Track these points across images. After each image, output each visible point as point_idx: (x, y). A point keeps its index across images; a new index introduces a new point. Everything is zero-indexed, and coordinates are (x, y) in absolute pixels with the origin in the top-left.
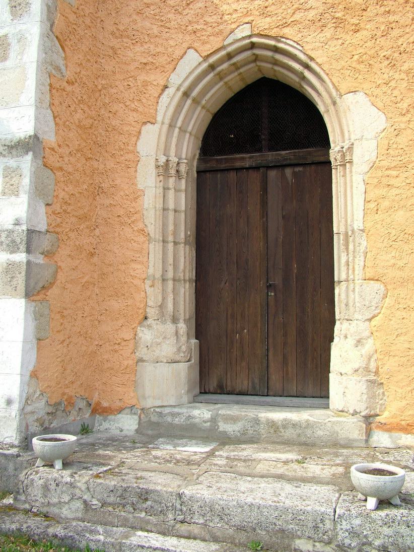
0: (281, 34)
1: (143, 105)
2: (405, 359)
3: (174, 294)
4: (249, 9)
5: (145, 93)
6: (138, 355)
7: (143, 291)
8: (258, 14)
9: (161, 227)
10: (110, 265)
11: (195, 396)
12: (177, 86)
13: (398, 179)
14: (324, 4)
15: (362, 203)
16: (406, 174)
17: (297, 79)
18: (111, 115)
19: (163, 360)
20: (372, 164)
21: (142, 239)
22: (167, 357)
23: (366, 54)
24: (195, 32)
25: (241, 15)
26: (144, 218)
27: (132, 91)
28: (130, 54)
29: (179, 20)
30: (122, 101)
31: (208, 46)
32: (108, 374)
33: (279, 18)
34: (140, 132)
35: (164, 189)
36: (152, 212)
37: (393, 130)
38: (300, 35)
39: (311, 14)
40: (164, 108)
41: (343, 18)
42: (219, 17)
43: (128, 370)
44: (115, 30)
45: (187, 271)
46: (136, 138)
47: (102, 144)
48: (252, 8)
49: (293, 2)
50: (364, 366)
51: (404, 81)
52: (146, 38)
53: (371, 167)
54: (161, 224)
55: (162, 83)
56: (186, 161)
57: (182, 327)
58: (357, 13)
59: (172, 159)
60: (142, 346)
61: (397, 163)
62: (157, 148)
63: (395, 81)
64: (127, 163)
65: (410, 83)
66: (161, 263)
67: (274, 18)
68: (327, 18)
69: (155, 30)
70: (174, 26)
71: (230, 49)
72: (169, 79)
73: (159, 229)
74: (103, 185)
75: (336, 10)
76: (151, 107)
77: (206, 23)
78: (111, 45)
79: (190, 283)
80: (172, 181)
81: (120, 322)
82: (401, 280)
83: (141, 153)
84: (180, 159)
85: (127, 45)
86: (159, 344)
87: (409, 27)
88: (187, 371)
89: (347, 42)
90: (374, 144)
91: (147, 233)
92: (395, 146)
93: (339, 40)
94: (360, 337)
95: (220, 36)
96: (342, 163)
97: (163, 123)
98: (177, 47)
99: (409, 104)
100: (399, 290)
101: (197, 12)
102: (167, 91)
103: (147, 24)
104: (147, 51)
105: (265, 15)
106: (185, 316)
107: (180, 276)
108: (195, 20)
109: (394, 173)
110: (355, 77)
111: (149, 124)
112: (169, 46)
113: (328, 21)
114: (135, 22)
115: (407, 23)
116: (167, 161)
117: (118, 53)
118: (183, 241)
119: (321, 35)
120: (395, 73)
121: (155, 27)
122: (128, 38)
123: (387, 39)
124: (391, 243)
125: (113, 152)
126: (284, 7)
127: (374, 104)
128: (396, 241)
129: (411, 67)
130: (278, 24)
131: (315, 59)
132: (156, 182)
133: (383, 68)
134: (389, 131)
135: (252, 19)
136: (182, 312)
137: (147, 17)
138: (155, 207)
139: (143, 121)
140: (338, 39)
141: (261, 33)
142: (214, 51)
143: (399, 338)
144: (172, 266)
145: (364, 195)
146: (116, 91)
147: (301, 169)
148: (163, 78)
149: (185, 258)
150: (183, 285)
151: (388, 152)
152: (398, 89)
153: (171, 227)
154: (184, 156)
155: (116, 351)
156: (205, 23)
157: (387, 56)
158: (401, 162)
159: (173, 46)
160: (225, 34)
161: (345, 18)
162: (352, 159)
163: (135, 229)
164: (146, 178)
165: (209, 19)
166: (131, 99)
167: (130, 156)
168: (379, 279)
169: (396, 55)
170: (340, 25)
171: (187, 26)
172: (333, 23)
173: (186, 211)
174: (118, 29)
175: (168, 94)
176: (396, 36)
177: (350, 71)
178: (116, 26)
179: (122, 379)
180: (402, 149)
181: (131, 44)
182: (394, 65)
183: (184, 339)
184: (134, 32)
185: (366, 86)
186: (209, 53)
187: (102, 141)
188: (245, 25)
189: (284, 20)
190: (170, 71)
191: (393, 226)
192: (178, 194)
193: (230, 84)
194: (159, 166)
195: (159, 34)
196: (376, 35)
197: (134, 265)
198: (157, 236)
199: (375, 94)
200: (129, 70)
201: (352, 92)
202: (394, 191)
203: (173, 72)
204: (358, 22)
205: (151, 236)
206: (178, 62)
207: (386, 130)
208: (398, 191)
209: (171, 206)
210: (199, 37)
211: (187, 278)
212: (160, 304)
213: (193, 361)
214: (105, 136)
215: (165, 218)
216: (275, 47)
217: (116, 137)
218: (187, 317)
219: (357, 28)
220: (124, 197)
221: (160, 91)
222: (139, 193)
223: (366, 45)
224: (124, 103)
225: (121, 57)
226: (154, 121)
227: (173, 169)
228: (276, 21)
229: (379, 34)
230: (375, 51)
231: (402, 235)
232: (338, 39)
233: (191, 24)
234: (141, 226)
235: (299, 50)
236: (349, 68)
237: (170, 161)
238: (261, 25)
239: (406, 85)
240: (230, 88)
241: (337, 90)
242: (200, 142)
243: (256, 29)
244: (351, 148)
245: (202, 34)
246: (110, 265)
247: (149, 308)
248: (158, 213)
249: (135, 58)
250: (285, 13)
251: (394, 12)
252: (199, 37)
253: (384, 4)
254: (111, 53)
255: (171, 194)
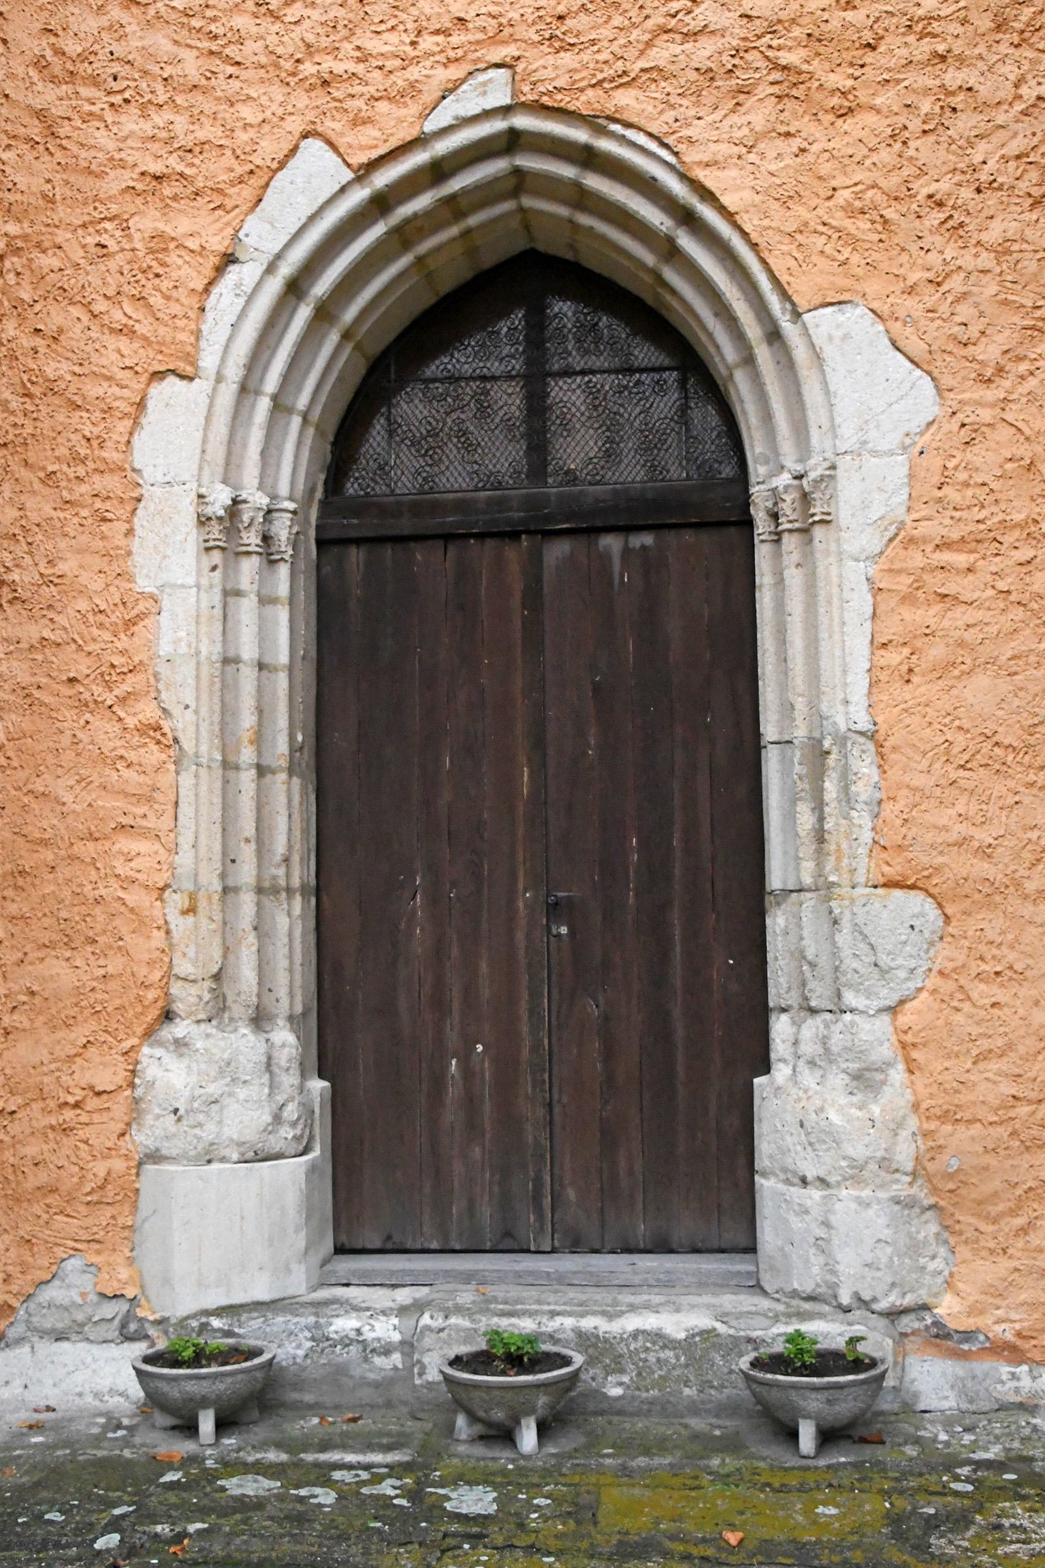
0: (610, 109)
1: (154, 315)
2: (1002, 1132)
3: (259, 937)
4: (504, 21)
5: (157, 276)
6: (143, 1138)
7: (159, 928)
8: (537, 38)
9: (217, 718)
10: (44, 842)
11: (325, 1263)
12: (264, 261)
13: (971, 577)
14: (745, 20)
15: (866, 651)
16: (996, 564)
17: (649, 259)
18: (39, 342)
19: (226, 1152)
20: (893, 529)
21: (153, 755)
22: (240, 1144)
23: (873, 187)
24: (325, 83)
25: (480, 36)
26: (161, 686)
27: (113, 264)
28: (102, 138)
29: (272, 39)
30: (78, 298)
31: (369, 134)
32: (37, 1209)
33: (602, 57)
34: (141, 405)
35: (226, 593)
36: (185, 673)
37: (955, 426)
38: (670, 116)
39: (704, 51)
40: (224, 331)
41: (805, 67)
42: (408, 41)
43: (110, 1190)
44: (49, 53)
45: (296, 858)
46: (128, 423)
47: (10, 437)
48: (516, 16)
49: (648, 4)
50: (879, 1154)
51: (989, 275)
52: (159, 87)
53: (891, 540)
54: (217, 708)
55: (218, 244)
56: (291, 506)
57: (284, 1038)
58: (847, 56)
59: (250, 499)
60: (157, 1111)
61: (969, 529)
62: (202, 460)
63: (963, 275)
64: (98, 504)
65: (1009, 285)
66: (219, 836)
67: (586, 57)
68: (755, 65)
69: (191, 66)
70: (255, 59)
71: (442, 147)
72: (241, 235)
73: (212, 724)
74: (17, 578)
75: (781, 41)
76: (180, 323)
77: (363, 57)
78: (38, 103)
79: (302, 895)
80: (249, 567)
81: (80, 1034)
82: (987, 889)
83: (145, 474)
84: (274, 497)
85: (93, 108)
86: (215, 1102)
87: (1006, 107)
88: (303, 1186)
89: (815, 148)
90: (899, 467)
91: (170, 736)
92: (962, 476)
93: (791, 140)
94: (863, 1065)
95: (409, 102)
96: (797, 525)
97: (219, 378)
98: (266, 128)
99: (1005, 348)
100: (980, 917)
101: (331, 15)
102: (233, 273)
103: (161, 41)
104: (163, 135)
105: (557, 45)
106: (291, 1004)
107: (274, 878)
108: (325, 42)
109: (961, 559)
110: (841, 258)
111: (172, 379)
112: (238, 124)
113: (757, 76)
114: (117, 30)
115: (1001, 95)
116: (235, 501)
117: (62, 132)
118: (284, 763)
119: (735, 119)
120: (963, 252)
121: (188, 55)
122: (96, 85)
123: (938, 143)
124: (953, 775)
125: (50, 468)
126: (618, 21)
127: (900, 344)
128: (969, 766)
129: (1009, 235)
130: (600, 76)
131: (718, 194)
132: (199, 572)
133: (926, 233)
134: (944, 430)
135: (516, 54)
136: (282, 992)
137: (158, 17)
138: (198, 653)
139: (151, 370)
140: (788, 135)
141: (545, 100)
142: (392, 152)
143: (981, 1066)
144: (253, 846)
145: (868, 625)
146: (56, 263)
147: (648, 539)
148: (221, 230)
149: (290, 816)
150: (285, 906)
151: (940, 494)
152: (971, 300)
153: (248, 720)
154: (284, 489)
155: (66, 1130)
156: (358, 54)
157: (938, 197)
158: (982, 527)
159: (251, 126)
160: (428, 98)
161: (811, 68)
162: (829, 514)
163: (131, 722)
164: (165, 557)
165: (373, 45)
166: (111, 292)
167: (110, 483)
168: (919, 884)
169: (967, 193)
170: (794, 92)
171: (298, 61)
172: (772, 83)
173: (291, 668)
174: (61, 53)
175: (238, 285)
176: (966, 135)
177: (823, 239)
178: (53, 40)
179: (89, 1222)
180: (984, 484)
181: (106, 106)
182: (961, 225)
183: (289, 1080)
184: (116, 68)
185: (873, 287)
186: (374, 154)
187: (11, 430)
188: (492, 73)
189: (620, 63)
190: (244, 208)
191: (957, 723)
192: (269, 609)
193: (432, 264)
194: (209, 519)
195: (204, 82)
196: (905, 128)
197: (126, 844)
198: (204, 748)
199: (901, 314)
200: (102, 196)
201: (832, 304)
202: (961, 616)
203: (252, 209)
204: (850, 83)
205: (185, 747)
206: (271, 178)
207: (935, 426)
208: (973, 615)
209: (248, 650)
210: (340, 101)
211: (296, 882)
212: (215, 970)
213: (316, 1153)
214: (20, 414)
215: (227, 689)
216: (588, 149)
217: (61, 417)
218: (299, 1009)
219: (847, 104)
220: (91, 618)
221: (208, 272)
222: (141, 607)
223: (875, 158)
224: (87, 306)
225: (75, 149)
226: (189, 370)
227: (253, 529)
228: (591, 65)
229: (915, 125)
230: (899, 180)
231: (988, 745)
232: (788, 135)
233: (311, 54)
234: (148, 711)
235: (666, 163)
236: (821, 228)
237: (245, 502)
238: (549, 73)
239: (993, 288)
240: (429, 276)
241: (785, 296)
242: (329, 447)
243: (526, 88)
244: (829, 477)
245: (351, 91)
246: (44, 842)
247: (180, 983)
248: (205, 671)
249: (123, 155)
250: (622, 41)
251: (961, 60)
252: (340, 101)
253: (929, 29)
254: (35, 130)
255: (247, 608)
